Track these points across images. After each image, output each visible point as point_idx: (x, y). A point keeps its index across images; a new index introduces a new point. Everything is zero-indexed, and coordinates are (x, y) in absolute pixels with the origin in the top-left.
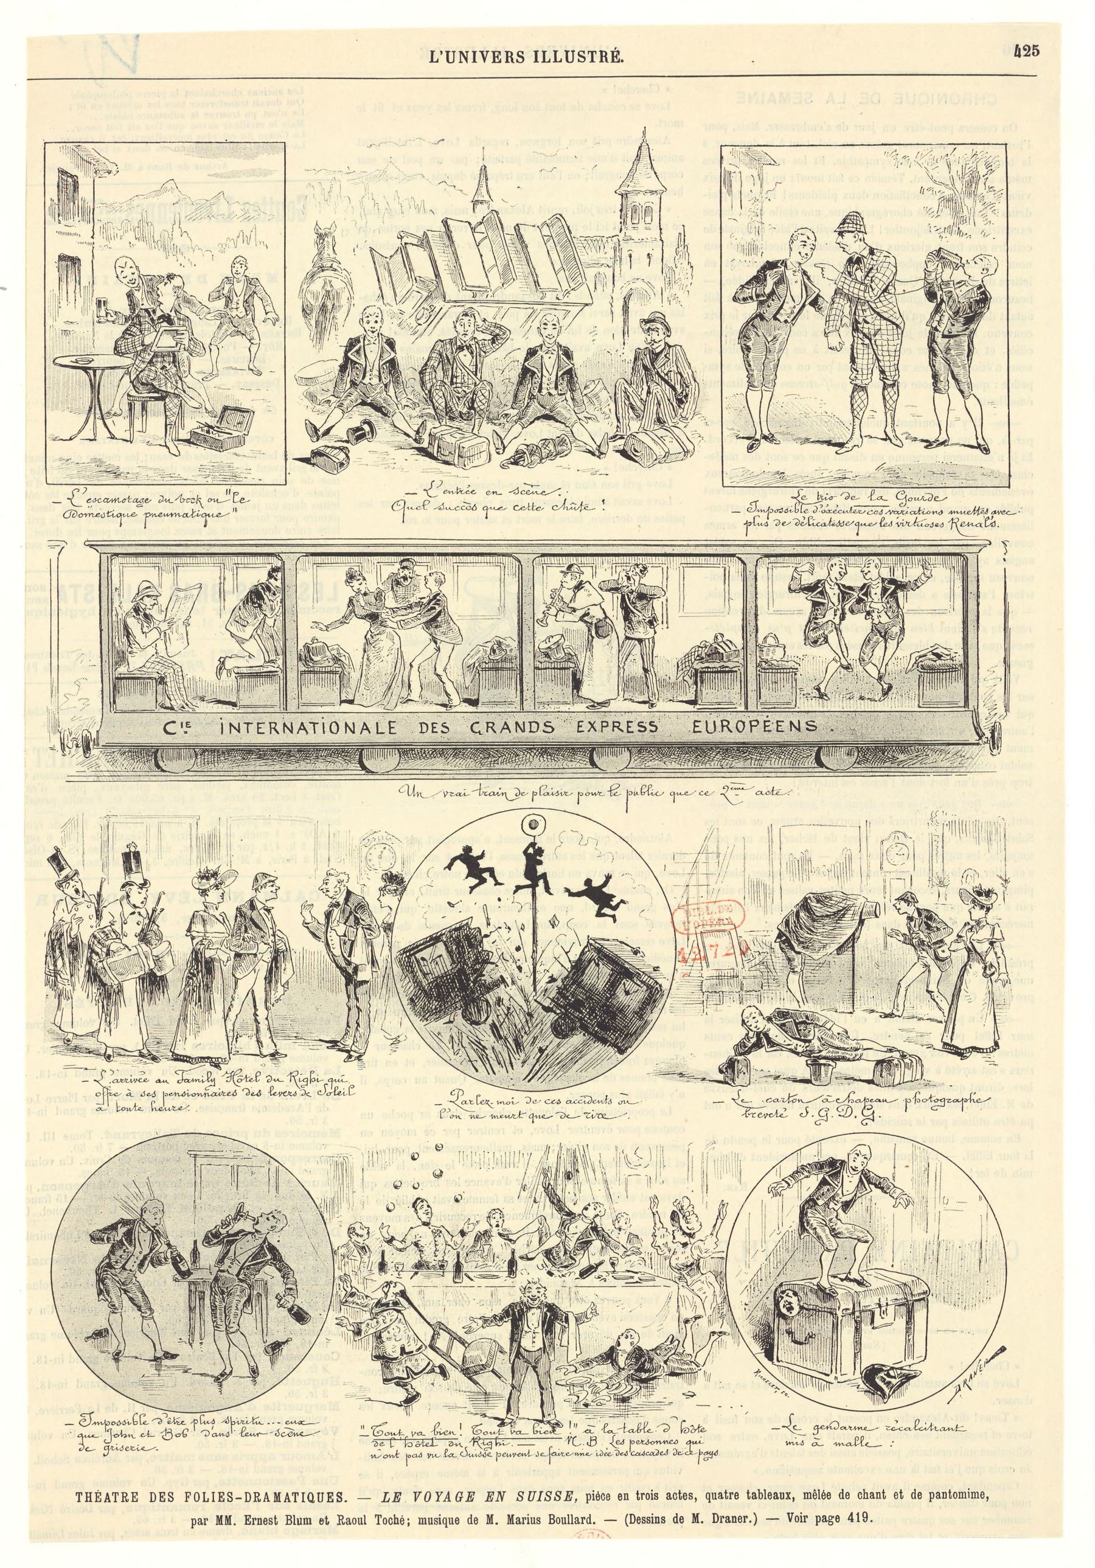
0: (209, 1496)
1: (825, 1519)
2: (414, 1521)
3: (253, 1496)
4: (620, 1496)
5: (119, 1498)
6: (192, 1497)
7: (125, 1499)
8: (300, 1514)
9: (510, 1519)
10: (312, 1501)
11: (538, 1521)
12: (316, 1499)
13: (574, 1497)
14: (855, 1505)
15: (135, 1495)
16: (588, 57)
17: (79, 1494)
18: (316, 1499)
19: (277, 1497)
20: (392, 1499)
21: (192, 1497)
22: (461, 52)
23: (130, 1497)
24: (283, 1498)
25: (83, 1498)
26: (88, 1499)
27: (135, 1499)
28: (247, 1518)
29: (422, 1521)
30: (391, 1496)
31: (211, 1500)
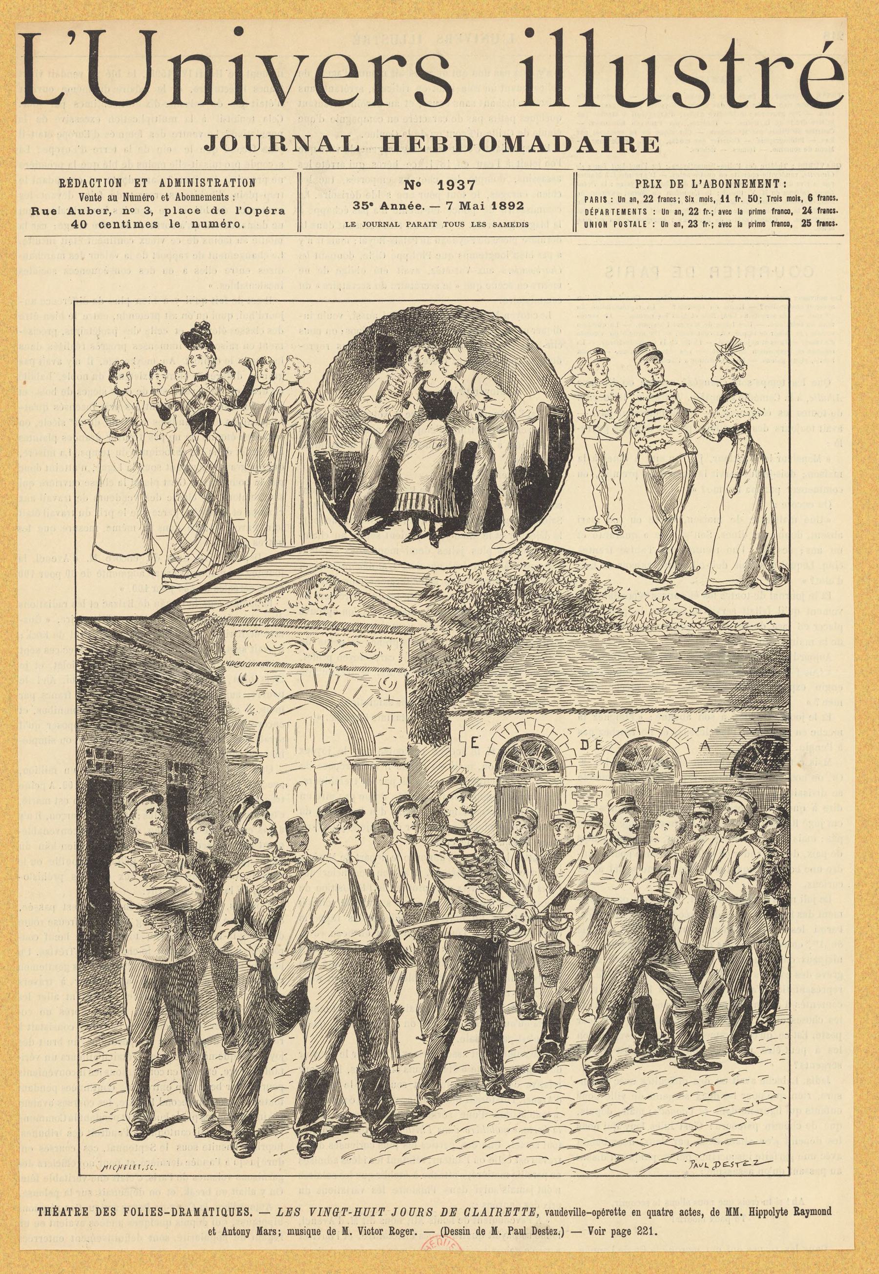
0: (143, 1211)
1: (619, 1232)
2: (284, 1232)
3: (103, 1210)
4: (633, 1212)
5: (73, 1212)
6: (129, 1212)
7: (77, 1214)
8: (518, 1226)
9: (259, 1230)
10: (225, 1216)
11: (318, 1232)
12: (228, 1213)
13: (536, 1212)
14: (643, 1221)
15: (85, 1209)
16: (207, 183)
17: (40, 1209)
18: (228, 1213)
19: (197, 1211)
20: (285, 1214)
21: (129, 1212)
22: (306, 148)
23: (81, 1212)
24: (201, 1212)
25: (43, 1212)
26: (48, 1213)
27: (85, 1214)
28: (510, 1229)
29: (290, 1232)
30: (284, 1211)
31: (145, 1214)
